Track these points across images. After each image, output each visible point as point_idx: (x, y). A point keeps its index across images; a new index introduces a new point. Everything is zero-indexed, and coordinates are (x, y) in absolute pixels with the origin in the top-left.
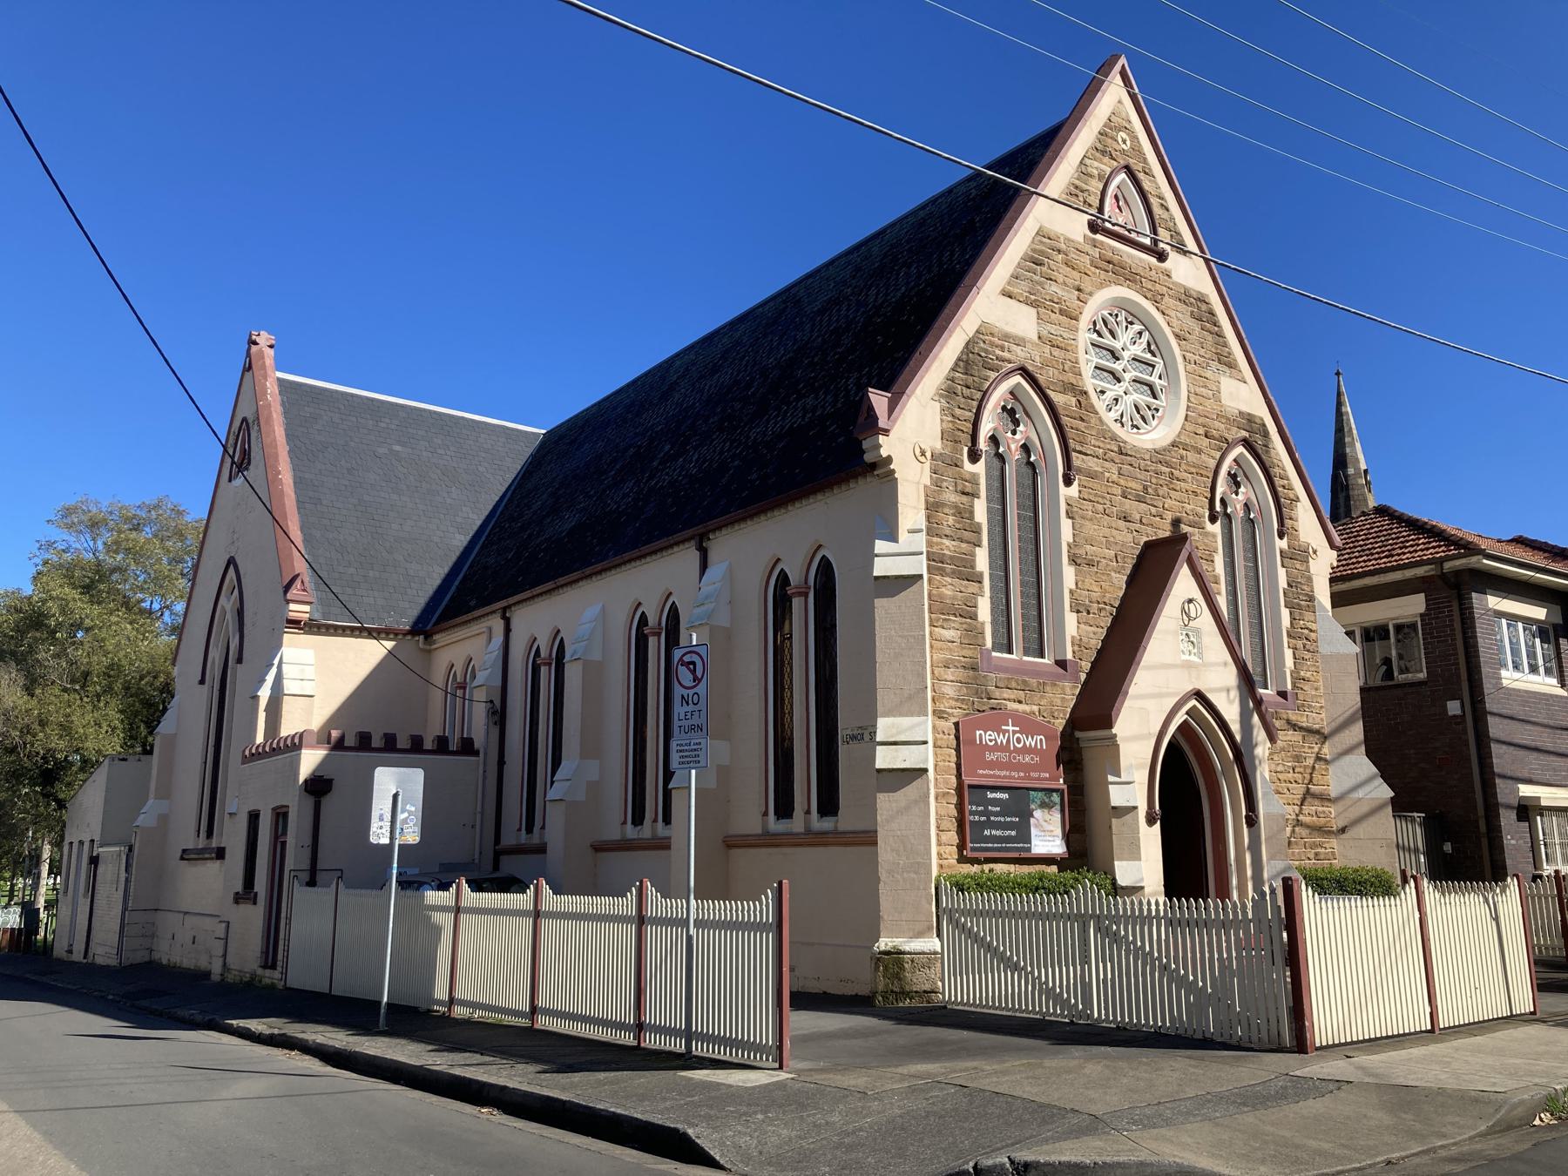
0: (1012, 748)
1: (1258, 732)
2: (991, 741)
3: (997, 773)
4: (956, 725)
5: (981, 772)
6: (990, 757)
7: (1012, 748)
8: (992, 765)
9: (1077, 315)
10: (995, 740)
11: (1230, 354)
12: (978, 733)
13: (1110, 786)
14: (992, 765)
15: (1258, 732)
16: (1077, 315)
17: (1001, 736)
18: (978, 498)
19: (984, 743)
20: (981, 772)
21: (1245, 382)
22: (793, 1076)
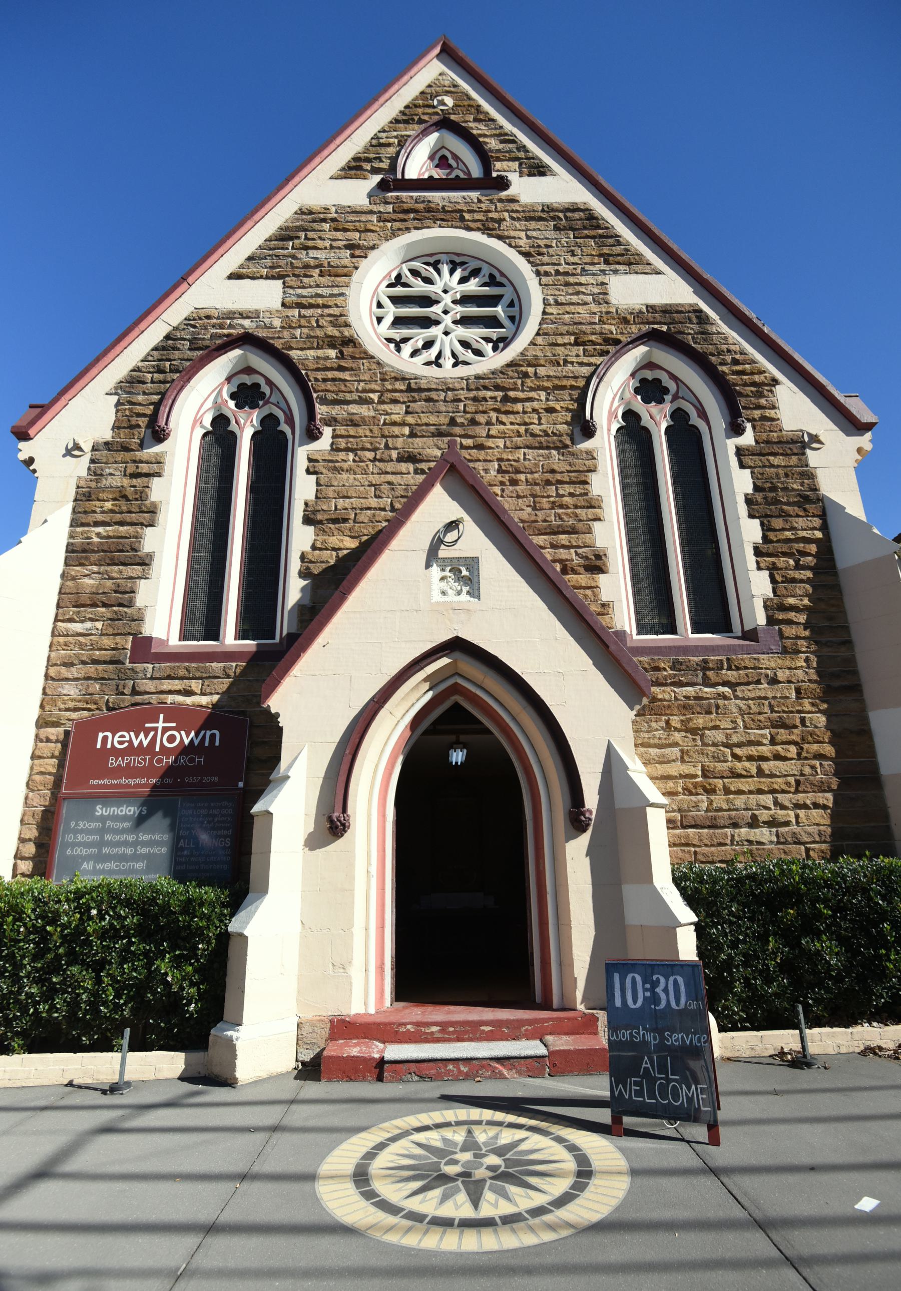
0: (157, 749)
1: (572, 1212)
2: (120, 743)
3: (123, 781)
4: (67, 733)
5: (95, 782)
6: (113, 762)
7: (157, 749)
8: (118, 772)
9: (132, 587)
10: (130, 742)
11: (627, 250)
12: (101, 735)
13: (649, 809)
14: (118, 772)
15: (572, 1212)
16: (132, 587)
17: (142, 736)
18: (520, 176)
19: (109, 746)
20: (95, 782)
21: (660, 273)
22: (491, 1028)
